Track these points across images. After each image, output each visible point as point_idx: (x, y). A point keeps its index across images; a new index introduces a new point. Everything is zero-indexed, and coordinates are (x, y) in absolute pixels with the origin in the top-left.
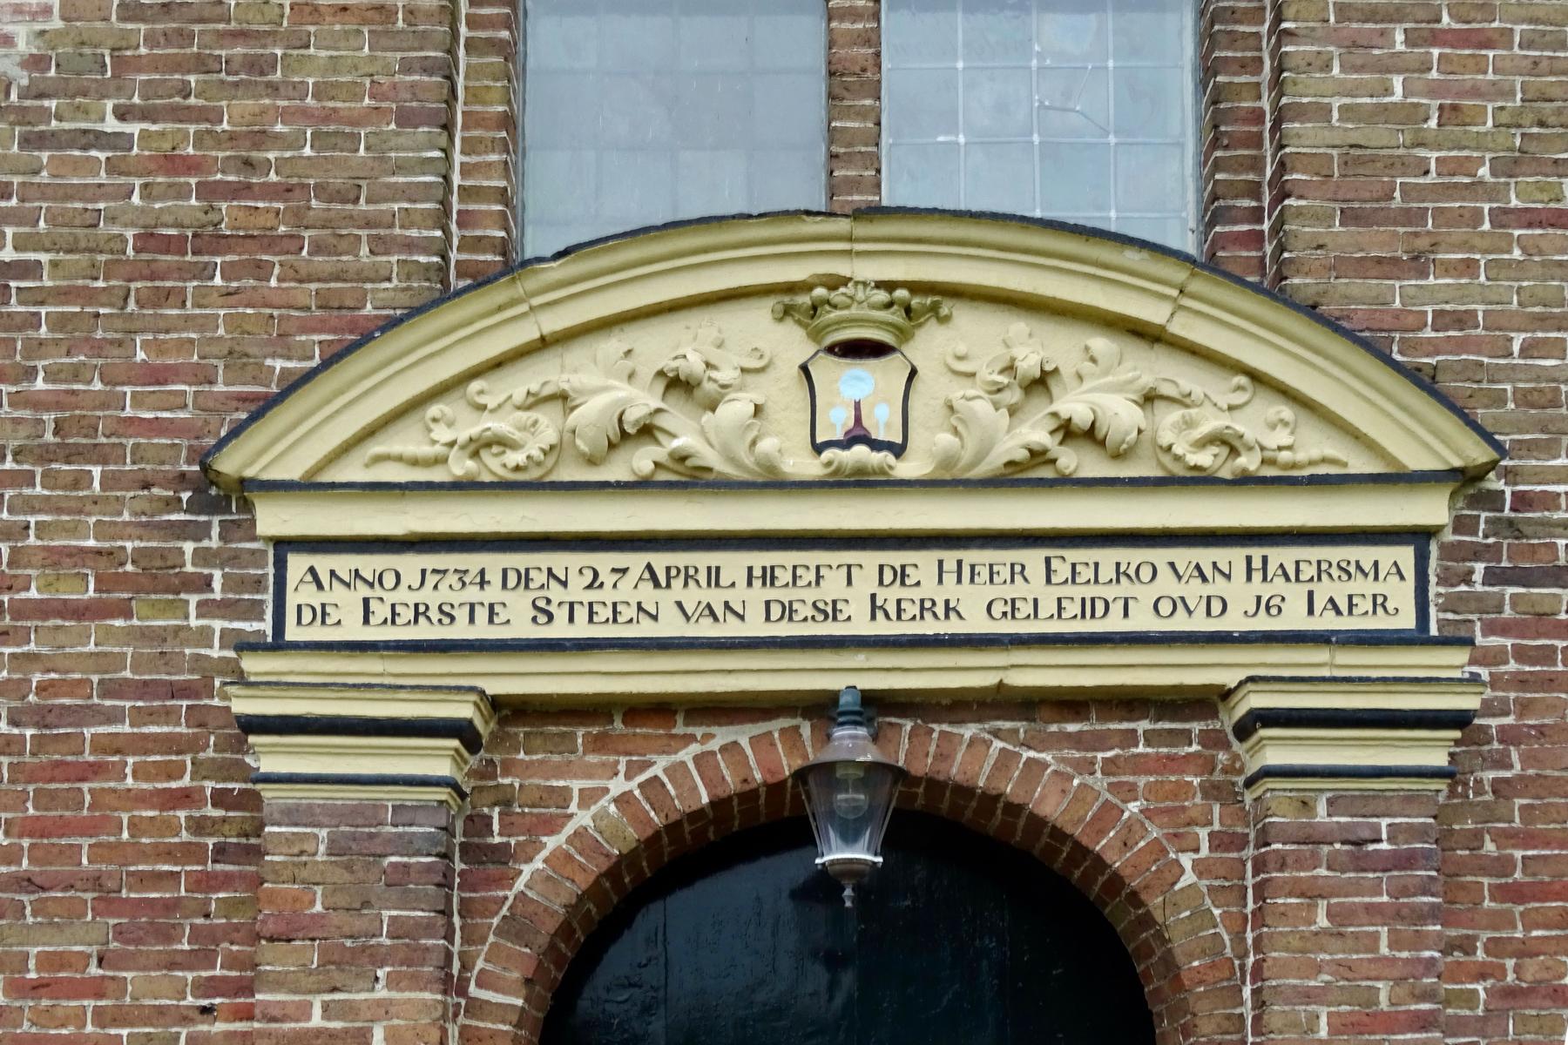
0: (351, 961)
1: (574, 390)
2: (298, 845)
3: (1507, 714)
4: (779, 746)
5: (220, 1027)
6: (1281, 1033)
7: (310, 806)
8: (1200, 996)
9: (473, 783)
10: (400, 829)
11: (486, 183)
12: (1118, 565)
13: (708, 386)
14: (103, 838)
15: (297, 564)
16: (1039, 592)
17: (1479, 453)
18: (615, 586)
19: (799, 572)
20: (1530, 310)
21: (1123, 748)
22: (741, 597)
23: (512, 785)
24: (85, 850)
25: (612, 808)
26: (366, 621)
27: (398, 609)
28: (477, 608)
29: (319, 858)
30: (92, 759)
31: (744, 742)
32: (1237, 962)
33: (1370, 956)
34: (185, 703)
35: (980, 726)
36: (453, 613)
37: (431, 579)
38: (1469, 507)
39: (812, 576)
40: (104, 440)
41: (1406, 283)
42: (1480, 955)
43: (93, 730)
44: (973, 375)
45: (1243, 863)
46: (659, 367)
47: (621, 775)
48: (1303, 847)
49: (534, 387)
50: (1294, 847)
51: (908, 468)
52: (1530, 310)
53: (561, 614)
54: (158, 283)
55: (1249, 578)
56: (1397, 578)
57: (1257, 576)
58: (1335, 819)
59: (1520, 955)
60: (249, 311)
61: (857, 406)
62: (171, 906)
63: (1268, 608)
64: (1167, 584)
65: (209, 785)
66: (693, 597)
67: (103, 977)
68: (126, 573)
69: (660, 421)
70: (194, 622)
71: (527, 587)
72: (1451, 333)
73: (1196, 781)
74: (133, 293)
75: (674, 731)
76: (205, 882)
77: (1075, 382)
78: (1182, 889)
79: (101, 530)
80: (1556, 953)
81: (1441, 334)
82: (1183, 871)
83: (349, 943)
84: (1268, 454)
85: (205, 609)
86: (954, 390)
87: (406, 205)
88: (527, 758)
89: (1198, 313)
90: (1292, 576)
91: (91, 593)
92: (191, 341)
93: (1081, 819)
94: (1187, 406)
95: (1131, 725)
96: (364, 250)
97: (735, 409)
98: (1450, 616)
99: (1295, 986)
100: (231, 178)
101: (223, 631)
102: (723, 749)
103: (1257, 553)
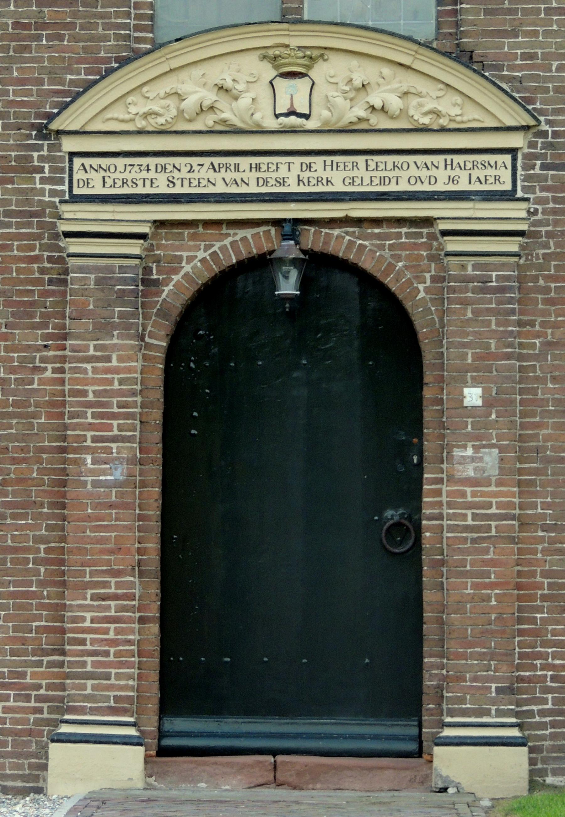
0: (104, 328)
1: (184, 93)
2: (82, 279)
3: (549, 226)
5: (51, 353)
6: (453, 360)
7: (87, 266)
8: (426, 344)
9: (146, 253)
10: (121, 275)
12: (394, 162)
14: (6, 276)
15: (78, 162)
16: (362, 175)
18: (199, 172)
21: (396, 240)
23: (160, 254)
26: (104, 186)
27: (116, 181)
28: (146, 180)
29: (91, 287)
31: (249, 237)
32: (441, 330)
33: (488, 329)
34: (36, 220)
35: (341, 230)
36: (137, 182)
37: (129, 168)
38: (534, 137)
39: (274, 167)
46: (216, 83)
47: (202, 250)
48: (463, 284)
50: (459, 284)
51: (311, 124)
53: (178, 183)
54: (22, 43)
55: (446, 169)
56: (504, 168)
57: (449, 167)
58: (475, 273)
59: (553, 328)
62: (32, 304)
63: (453, 181)
64: (413, 171)
65: (46, 254)
66: (230, 176)
67: (7, 332)
68: (12, 165)
69: (217, 105)
70: (38, 186)
71: (165, 172)
73: (425, 254)
74: (12, 47)
75: (222, 232)
76: (45, 294)
77: (377, 87)
78: (419, 299)
82: (419, 291)
83: (103, 321)
84: (452, 118)
85: (43, 180)
87: (116, 9)
88: (166, 243)
90: (463, 168)
93: (380, 270)
94: (421, 97)
96: (100, 29)
97: (245, 102)
98: (526, 184)
99: (459, 341)
102: (241, 239)
103: (449, 157)
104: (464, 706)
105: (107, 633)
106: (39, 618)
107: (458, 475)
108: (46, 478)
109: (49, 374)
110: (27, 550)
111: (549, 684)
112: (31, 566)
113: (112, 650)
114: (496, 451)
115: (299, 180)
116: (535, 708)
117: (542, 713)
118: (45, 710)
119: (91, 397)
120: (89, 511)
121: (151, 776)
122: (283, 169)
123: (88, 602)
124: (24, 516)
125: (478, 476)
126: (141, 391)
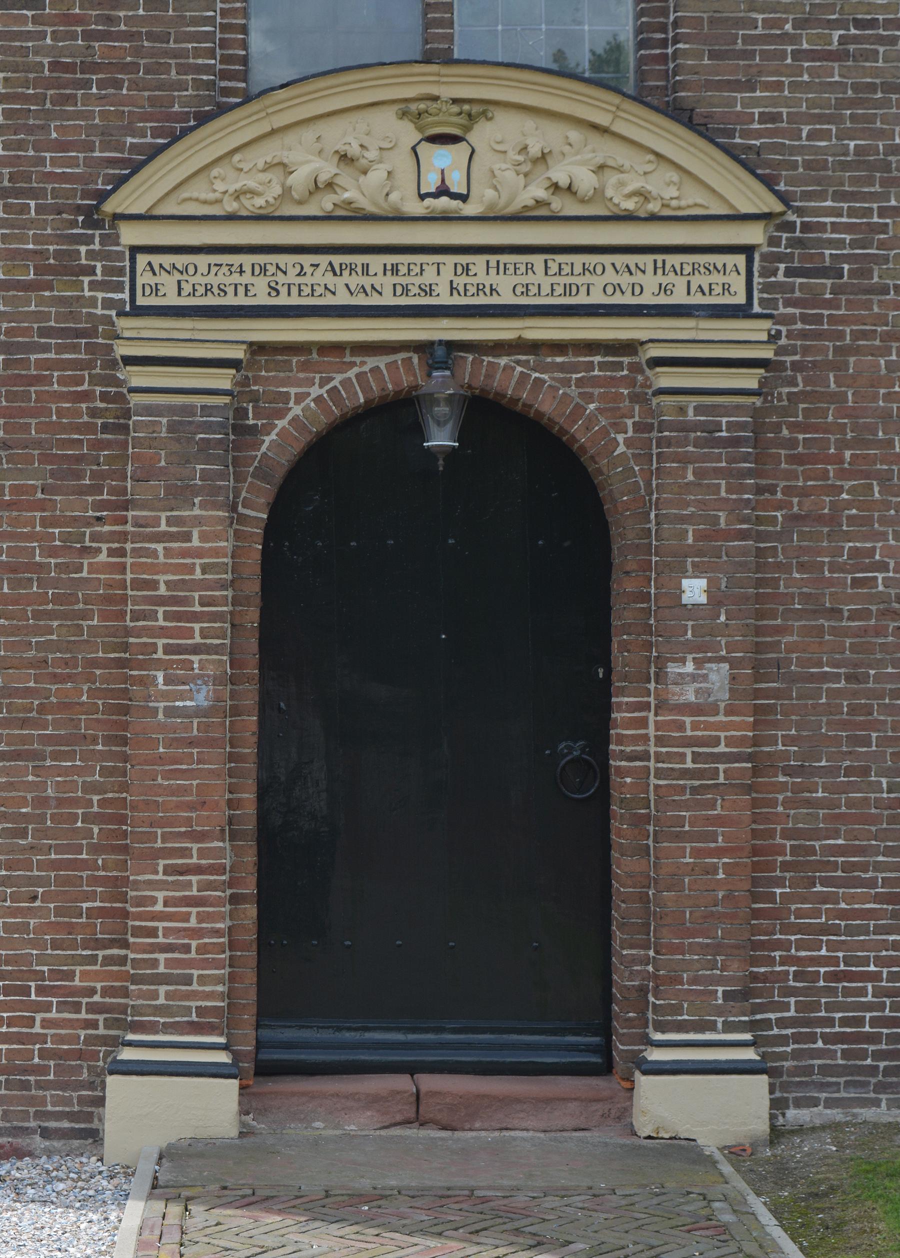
0: (180, 494)
3: (796, 354)
4: (401, 369)
5: (107, 528)
9: (238, 389)
10: (205, 419)
11: (234, 21)
12: (584, 264)
13: (363, 162)
15: (142, 260)
16: (542, 282)
17: (778, 207)
19: (412, 267)
20: (812, 111)
22: (380, 283)
23: (258, 390)
24: (33, 426)
25: (312, 404)
26: (179, 294)
27: (197, 287)
29: (162, 435)
30: (35, 373)
31: (383, 367)
34: (84, 341)
36: (226, 289)
37: (214, 269)
38: (777, 230)
39: (418, 270)
40: (35, 185)
41: (744, 95)
42: (779, 495)
43: (35, 356)
44: (505, 152)
45: (651, 440)
47: (317, 385)
48: (681, 434)
49: (269, 159)
51: (470, 209)
52: (812, 111)
53: (284, 291)
54: (62, 91)
55: (655, 273)
56: (736, 273)
57: (660, 271)
58: (698, 418)
60: (112, 109)
61: (443, 171)
62: (79, 459)
63: (665, 291)
64: (610, 276)
65: (98, 389)
66: (355, 281)
67: (45, 499)
69: (338, 180)
70: (87, 293)
71: (265, 275)
72: (768, 126)
73: (626, 392)
75: (345, 360)
79: (37, 240)
80: (821, 495)
81: (763, 126)
82: (618, 445)
83: (179, 483)
84: (665, 202)
85: (93, 286)
86: (497, 164)
89: (626, 120)
90: (679, 273)
91: (32, 276)
92: (81, 126)
94: (622, 172)
95: (591, 359)
96: (173, 72)
97: (377, 175)
100: (100, 28)
101: (103, 298)
102: (371, 370)
103: (660, 258)
104: (679, 1018)
105: (188, 921)
106: (88, 897)
107: (674, 700)
108: (100, 702)
109: (103, 557)
110: (74, 802)
111: (791, 983)
112: (79, 824)
113: (194, 944)
114: (726, 666)
115: (452, 288)
116: (772, 1016)
117: (782, 1023)
118: (101, 1024)
119: (163, 590)
120: (161, 750)
121: (248, 1114)
122: (430, 271)
123: (160, 877)
124: (70, 756)
125: (701, 701)
126: (232, 581)
